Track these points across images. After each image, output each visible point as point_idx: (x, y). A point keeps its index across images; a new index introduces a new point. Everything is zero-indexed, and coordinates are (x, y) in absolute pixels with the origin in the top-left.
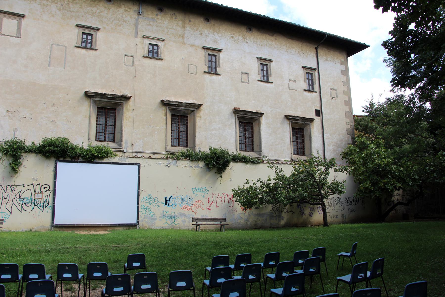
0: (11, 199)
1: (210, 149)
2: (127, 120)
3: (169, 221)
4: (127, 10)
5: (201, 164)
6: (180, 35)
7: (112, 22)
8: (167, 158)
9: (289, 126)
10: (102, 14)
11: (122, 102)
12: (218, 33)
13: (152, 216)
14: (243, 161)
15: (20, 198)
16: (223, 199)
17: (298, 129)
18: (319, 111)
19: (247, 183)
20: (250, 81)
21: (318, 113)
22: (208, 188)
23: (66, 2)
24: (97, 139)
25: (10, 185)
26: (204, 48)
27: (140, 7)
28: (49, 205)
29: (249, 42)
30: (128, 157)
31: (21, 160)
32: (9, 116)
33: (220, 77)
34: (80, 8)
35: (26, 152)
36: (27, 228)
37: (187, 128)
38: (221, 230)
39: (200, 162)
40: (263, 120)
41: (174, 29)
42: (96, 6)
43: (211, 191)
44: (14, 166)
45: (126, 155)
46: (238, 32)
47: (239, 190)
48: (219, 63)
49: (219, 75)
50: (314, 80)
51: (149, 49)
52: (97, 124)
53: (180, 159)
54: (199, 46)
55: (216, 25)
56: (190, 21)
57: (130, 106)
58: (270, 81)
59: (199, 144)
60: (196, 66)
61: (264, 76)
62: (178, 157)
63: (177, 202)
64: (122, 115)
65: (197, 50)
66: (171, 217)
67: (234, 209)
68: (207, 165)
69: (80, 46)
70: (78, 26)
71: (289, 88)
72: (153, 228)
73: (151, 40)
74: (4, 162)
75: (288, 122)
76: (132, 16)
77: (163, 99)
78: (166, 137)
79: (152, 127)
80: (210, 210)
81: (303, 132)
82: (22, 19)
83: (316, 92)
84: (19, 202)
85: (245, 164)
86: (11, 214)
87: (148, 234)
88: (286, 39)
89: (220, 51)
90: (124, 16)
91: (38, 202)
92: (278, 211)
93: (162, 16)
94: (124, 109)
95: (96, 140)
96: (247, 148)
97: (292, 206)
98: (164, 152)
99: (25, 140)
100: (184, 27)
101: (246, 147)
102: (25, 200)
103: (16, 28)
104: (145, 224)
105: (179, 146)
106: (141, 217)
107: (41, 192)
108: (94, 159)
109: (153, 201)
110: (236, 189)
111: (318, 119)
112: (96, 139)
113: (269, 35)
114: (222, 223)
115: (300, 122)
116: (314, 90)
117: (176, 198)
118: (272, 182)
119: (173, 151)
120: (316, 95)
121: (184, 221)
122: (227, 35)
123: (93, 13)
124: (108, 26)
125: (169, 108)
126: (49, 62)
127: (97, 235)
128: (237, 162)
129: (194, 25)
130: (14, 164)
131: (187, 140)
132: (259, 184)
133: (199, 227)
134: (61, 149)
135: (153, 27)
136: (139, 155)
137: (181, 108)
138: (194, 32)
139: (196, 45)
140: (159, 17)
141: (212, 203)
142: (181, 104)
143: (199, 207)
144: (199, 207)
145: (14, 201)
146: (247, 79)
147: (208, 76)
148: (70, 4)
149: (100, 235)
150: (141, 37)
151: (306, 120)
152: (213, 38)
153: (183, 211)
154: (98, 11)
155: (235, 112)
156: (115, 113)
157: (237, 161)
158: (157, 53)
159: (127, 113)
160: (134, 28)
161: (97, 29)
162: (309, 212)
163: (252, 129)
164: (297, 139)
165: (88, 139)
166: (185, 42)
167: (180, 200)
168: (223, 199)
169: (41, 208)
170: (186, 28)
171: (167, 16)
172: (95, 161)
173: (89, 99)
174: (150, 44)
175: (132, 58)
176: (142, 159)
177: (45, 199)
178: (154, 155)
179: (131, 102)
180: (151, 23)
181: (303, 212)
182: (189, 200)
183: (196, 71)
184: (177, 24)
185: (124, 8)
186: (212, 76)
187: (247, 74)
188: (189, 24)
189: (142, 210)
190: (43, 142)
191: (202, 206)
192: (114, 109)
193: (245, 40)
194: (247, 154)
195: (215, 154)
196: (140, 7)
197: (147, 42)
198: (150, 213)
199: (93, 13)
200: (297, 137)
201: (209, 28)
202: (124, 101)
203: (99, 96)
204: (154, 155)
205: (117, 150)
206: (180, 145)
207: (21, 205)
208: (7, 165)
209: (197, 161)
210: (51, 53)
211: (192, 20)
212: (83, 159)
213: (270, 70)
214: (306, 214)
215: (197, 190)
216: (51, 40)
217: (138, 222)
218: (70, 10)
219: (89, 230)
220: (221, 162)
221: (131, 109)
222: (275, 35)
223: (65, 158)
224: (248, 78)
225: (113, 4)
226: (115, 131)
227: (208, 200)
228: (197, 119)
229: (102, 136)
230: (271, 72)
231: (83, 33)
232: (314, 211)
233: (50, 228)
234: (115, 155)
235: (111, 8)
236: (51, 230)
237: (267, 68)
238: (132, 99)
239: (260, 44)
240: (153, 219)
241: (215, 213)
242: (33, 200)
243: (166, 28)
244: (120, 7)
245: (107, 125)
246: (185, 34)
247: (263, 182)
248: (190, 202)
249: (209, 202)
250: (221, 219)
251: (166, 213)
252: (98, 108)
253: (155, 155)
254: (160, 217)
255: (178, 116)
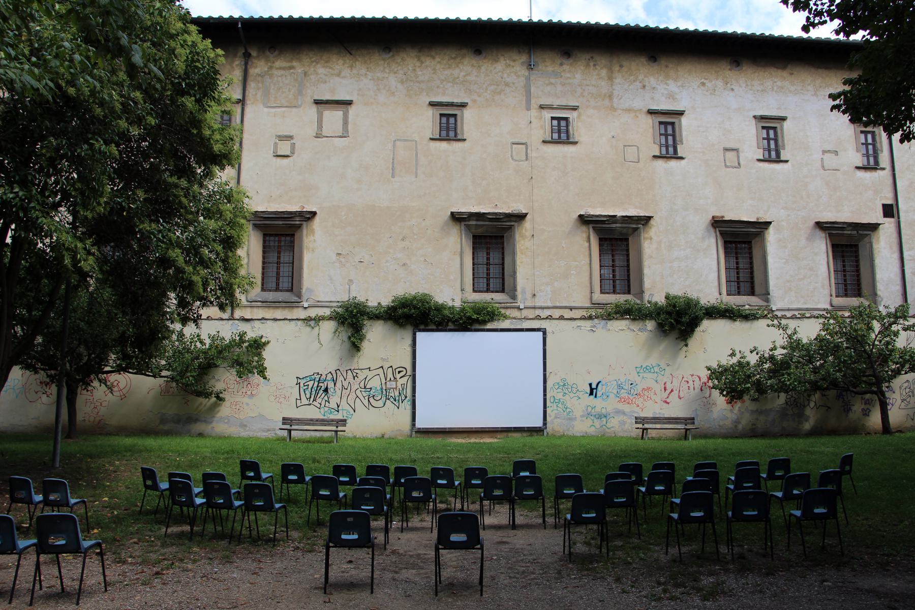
0: (353, 390)
1: (666, 298)
2: (522, 253)
3: (597, 423)
4: (509, 65)
5: (650, 325)
6: (605, 95)
7: (487, 89)
8: (590, 318)
9: (824, 242)
10: (468, 78)
11: (512, 224)
12: (675, 80)
13: (568, 414)
14: (727, 316)
15: (365, 388)
16: (691, 383)
17: (847, 245)
18: (891, 206)
19: (733, 355)
20: (742, 162)
21: (889, 211)
22: (663, 365)
23: (410, 68)
24: (475, 289)
25: (351, 369)
26: (651, 112)
27: (530, 56)
28: (408, 398)
29: (736, 88)
30: (526, 319)
31: (364, 331)
32: (341, 262)
33: (683, 162)
34: (433, 73)
35: (370, 318)
36: (377, 432)
37: (628, 260)
38: (686, 438)
39: (647, 321)
40: (771, 236)
41: (593, 85)
42: (458, 66)
43: (668, 370)
44: (355, 340)
45: (525, 313)
46: (713, 72)
47: (719, 368)
48: (681, 136)
49: (682, 158)
50: (878, 145)
51: (552, 126)
52: (474, 264)
53: (614, 317)
54: (641, 110)
55: (670, 65)
56: (621, 66)
57: (526, 230)
58: (782, 158)
59: (649, 287)
60: (638, 148)
61: (769, 151)
62: (609, 315)
63: (610, 391)
64: (514, 245)
65: (637, 117)
66: (600, 416)
67: (711, 402)
68: (660, 326)
69: (438, 137)
70: (432, 104)
71: (823, 167)
72: (570, 434)
73: (554, 111)
74: (340, 334)
75: (824, 235)
76: (519, 73)
77: (582, 213)
78: (591, 278)
79: (566, 263)
80: (668, 403)
81: (857, 252)
82: (349, 106)
83: (883, 169)
84: (365, 394)
85: (730, 321)
86: (354, 411)
87: (559, 442)
88: (813, 70)
89: (681, 113)
90: (505, 76)
91: (391, 395)
92: (796, 404)
93: (571, 65)
94: (517, 236)
95: (474, 291)
96: (742, 289)
97: (825, 395)
98: (588, 305)
99: (367, 300)
100: (610, 78)
101: (739, 288)
102: (373, 390)
103: (341, 122)
104: (557, 428)
105: (614, 292)
106: (550, 416)
107: (395, 378)
108: (471, 324)
109: (570, 390)
110: (714, 365)
111: (890, 223)
112: (601, 290)
113: (777, 68)
114: (689, 427)
115: (849, 232)
116: (878, 165)
117: (609, 384)
118: (779, 353)
119: (605, 302)
120: (885, 175)
121: (624, 423)
122: (693, 82)
123: (455, 79)
124: (479, 96)
125: (593, 227)
126: (393, 170)
127: (480, 443)
128: (715, 318)
129: (629, 73)
130: (355, 337)
131: (629, 281)
132: (753, 359)
133: (647, 432)
134: (421, 312)
135: (556, 87)
136: (547, 313)
137: (614, 226)
138: (630, 85)
139: (635, 109)
140: (566, 67)
141: (672, 391)
142: (614, 219)
143: (649, 399)
144: (649, 399)
145: (358, 392)
146: (736, 159)
147: (660, 163)
148: (418, 70)
149: (485, 443)
150: (537, 107)
151: (861, 226)
152: (666, 92)
153: (621, 406)
154: (462, 74)
155: (714, 224)
156: (503, 244)
157: (715, 317)
158: (567, 132)
159: (522, 242)
160: (524, 93)
161: (463, 105)
162: (863, 406)
163: (751, 253)
164: (844, 266)
165: (460, 289)
166: (615, 105)
167: (616, 387)
168: (691, 383)
169: (395, 403)
170: (614, 80)
171: (579, 63)
172: (473, 328)
173: (458, 224)
174: (553, 118)
175: (524, 146)
176: (548, 320)
177: (401, 389)
178: (571, 310)
179: (527, 224)
180: (553, 81)
181: (850, 408)
182: (630, 386)
183: (638, 156)
184: (598, 75)
185: (505, 62)
186: (668, 162)
187: (737, 150)
188: (619, 71)
189: (552, 405)
190: (393, 301)
191: (654, 397)
192: (500, 236)
193: (729, 85)
194: (735, 301)
195: (674, 306)
196: (530, 56)
197: (548, 115)
198: (564, 409)
199: (455, 79)
200: (844, 261)
201: (657, 73)
202: (515, 221)
203: (475, 218)
204: (571, 310)
205: (509, 305)
206: (618, 291)
207: (367, 398)
208: (346, 339)
209: (642, 319)
210: (394, 155)
211: (625, 63)
212: (455, 325)
213: (783, 137)
214: (855, 411)
215: (645, 370)
216: (393, 134)
217: (545, 424)
218: (418, 79)
219: (468, 437)
220: (685, 319)
221: (528, 234)
222: (789, 66)
223: (426, 325)
224: (738, 157)
225: (485, 58)
226: (503, 274)
227: (663, 386)
228: (644, 243)
229: (483, 284)
230: (783, 141)
231: (442, 115)
232: (873, 406)
233: (409, 434)
234: (504, 317)
235: (482, 66)
236: (411, 436)
237: (776, 134)
238: (528, 217)
239: (759, 88)
240: (571, 419)
241: (676, 409)
242: (384, 391)
243: (579, 85)
244: (497, 61)
245: (490, 264)
246: (614, 92)
247: (762, 353)
248: (632, 391)
249: (665, 389)
250: (686, 419)
251: (592, 409)
252: (475, 237)
253: (573, 310)
254: (582, 416)
255: (611, 239)
